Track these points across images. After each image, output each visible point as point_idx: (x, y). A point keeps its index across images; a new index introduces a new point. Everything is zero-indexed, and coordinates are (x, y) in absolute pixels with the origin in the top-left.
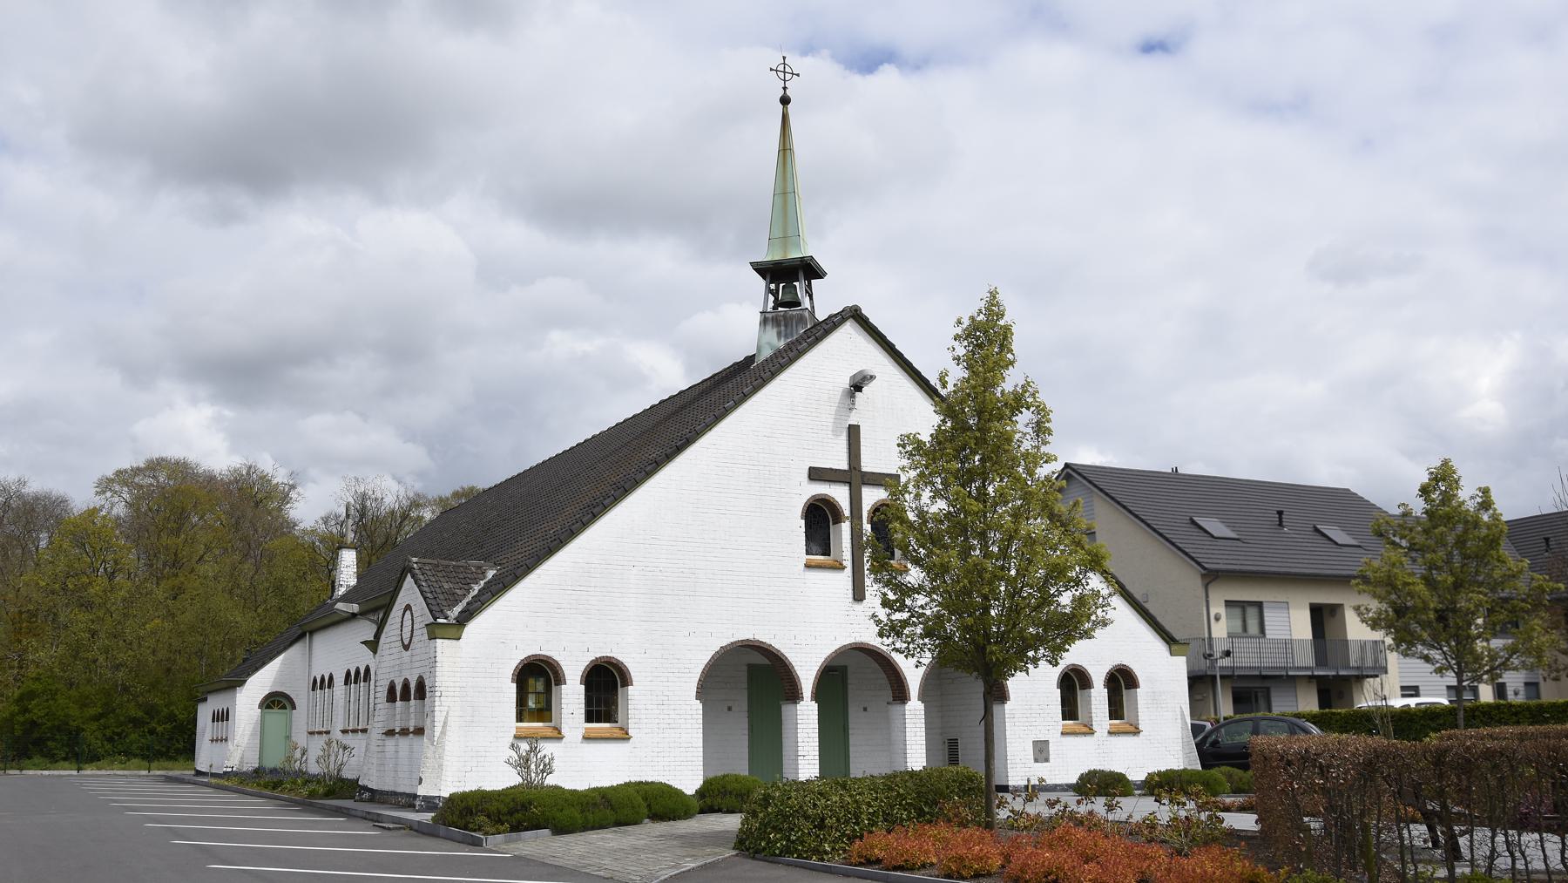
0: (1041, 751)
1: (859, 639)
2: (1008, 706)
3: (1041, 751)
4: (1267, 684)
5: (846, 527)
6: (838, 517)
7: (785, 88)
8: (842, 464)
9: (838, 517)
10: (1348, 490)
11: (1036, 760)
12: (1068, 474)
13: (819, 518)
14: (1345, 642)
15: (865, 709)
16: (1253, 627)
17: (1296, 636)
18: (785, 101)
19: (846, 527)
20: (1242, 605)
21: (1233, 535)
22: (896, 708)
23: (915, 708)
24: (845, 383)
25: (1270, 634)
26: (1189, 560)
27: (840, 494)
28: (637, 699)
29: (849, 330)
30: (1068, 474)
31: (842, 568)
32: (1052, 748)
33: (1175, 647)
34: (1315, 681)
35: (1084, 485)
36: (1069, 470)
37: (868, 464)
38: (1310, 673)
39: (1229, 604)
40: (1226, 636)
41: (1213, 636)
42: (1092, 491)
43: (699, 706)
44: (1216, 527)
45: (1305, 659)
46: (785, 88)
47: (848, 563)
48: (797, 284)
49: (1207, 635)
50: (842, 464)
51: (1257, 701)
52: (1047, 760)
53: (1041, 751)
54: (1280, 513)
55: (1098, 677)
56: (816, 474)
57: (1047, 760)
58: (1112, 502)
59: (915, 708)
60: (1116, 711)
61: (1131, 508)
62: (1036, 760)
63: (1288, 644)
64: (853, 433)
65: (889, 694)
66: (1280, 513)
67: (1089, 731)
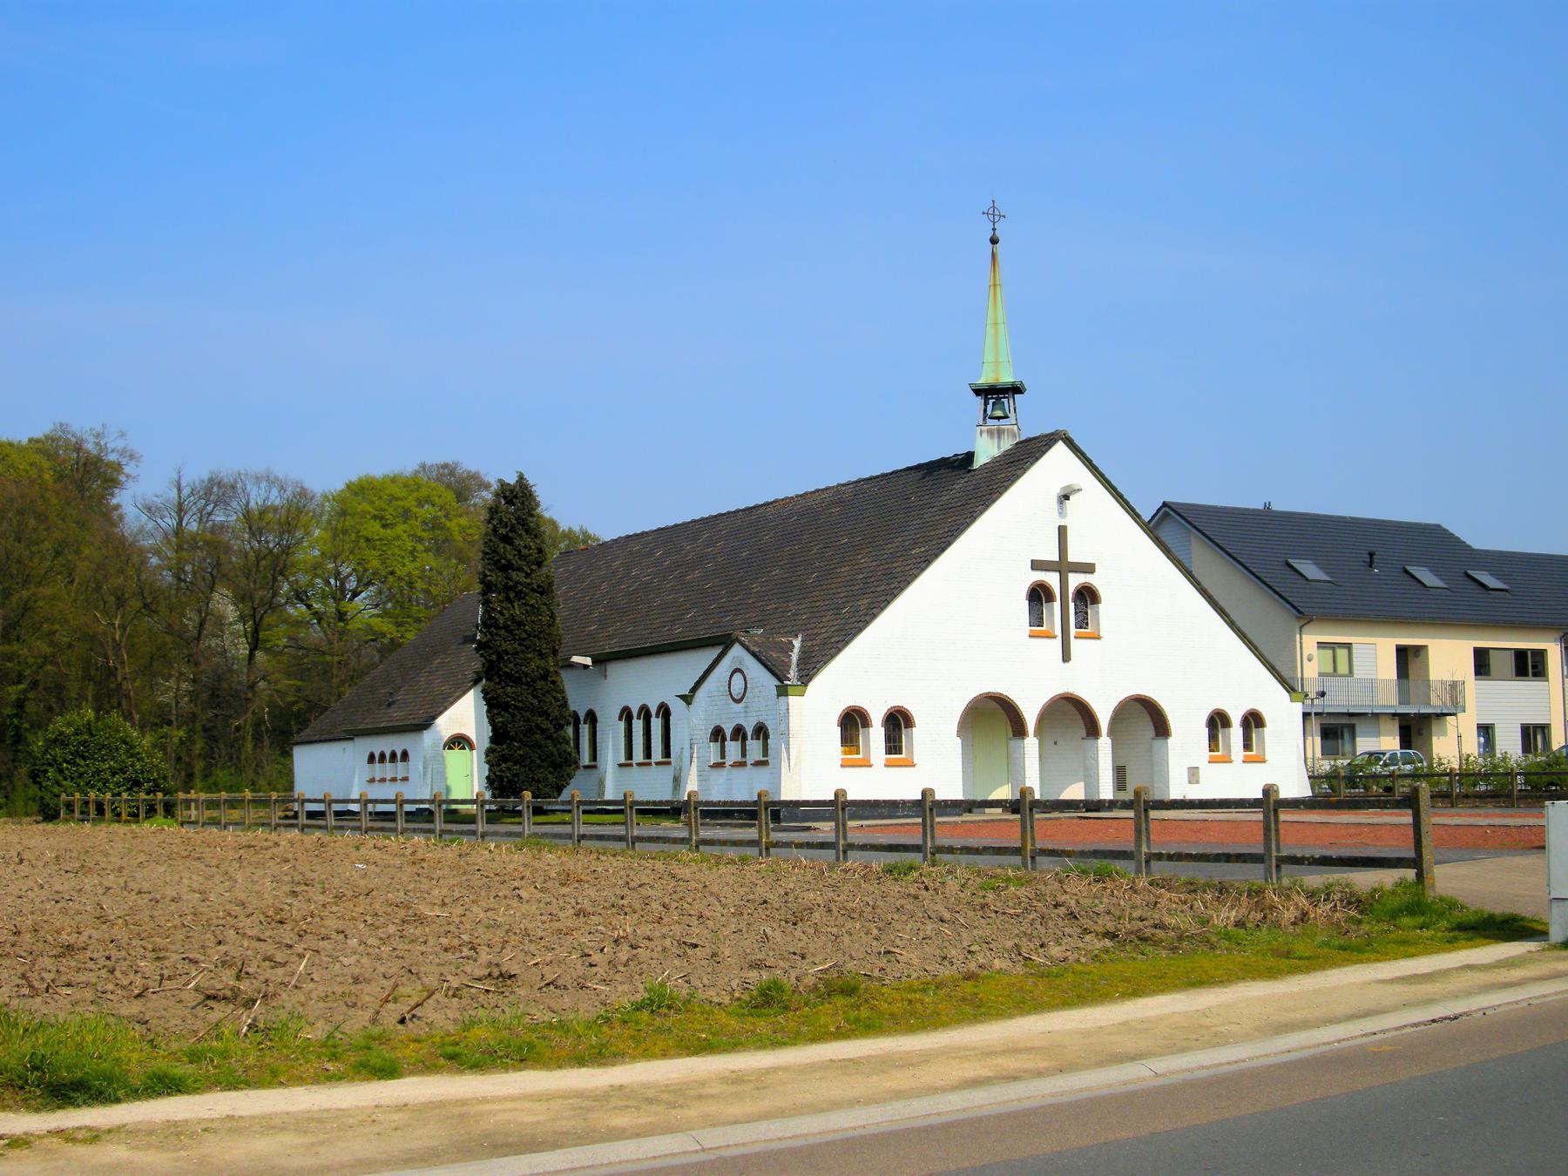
0: (1193, 775)
1: (1071, 690)
2: (1170, 741)
3: (1193, 775)
4: (1353, 721)
5: (1057, 605)
6: (1050, 598)
7: (994, 229)
8: (1054, 556)
9: (1050, 598)
10: (1439, 526)
11: (1190, 782)
12: (1166, 512)
13: (1038, 596)
14: (1427, 681)
15: (1055, 743)
16: (1343, 667)
17: (1381, 676)
18: (994, 241)
19: (1057, 605)
20: (1333, 646)
21: (1328, 579)
22: (1158, 742)
23: (1104, 743)
24: (1056, 491)
25: (1357, 673)
26: (1237, 565)
27: (1052, 579)
28: (919, 738)
29: (1060, 448)
30: (1166, 512)
31: (1055, 637)
32: (1201, 773)
33: (1293, 694)
34: (1397, 718)
35: (1182, 524)
36: (1167, 510)
37: (1073, 556)
38: (1393, 711)
39: (1321, 645)
40: (1317, 676)
41: (1305, 676)
42: (1190, 531)
43: (959, 741)
44: (1310, 570)
45: (1388, 699)
46: (994, 229)
47: (1058, 631)
48: (1005, 400)
49: (1299, 676)
50: (1054, 556)
51: (1342, 738)
52: (1198, 782)
53: (1193, 775)
54: (1371, 555)
55: (1236, 719)
56: (1037, 565)
57: (1198, 782)
58: (1258, 581)
59: (1104, 743)
60: (1247, 746)
61: (1230, 551)
62: (1190, 782)
63: (1372, 684)
64: (1062, 531)
65: (1151, 731)
66: (1371, 555)
67: (1227, 760)
